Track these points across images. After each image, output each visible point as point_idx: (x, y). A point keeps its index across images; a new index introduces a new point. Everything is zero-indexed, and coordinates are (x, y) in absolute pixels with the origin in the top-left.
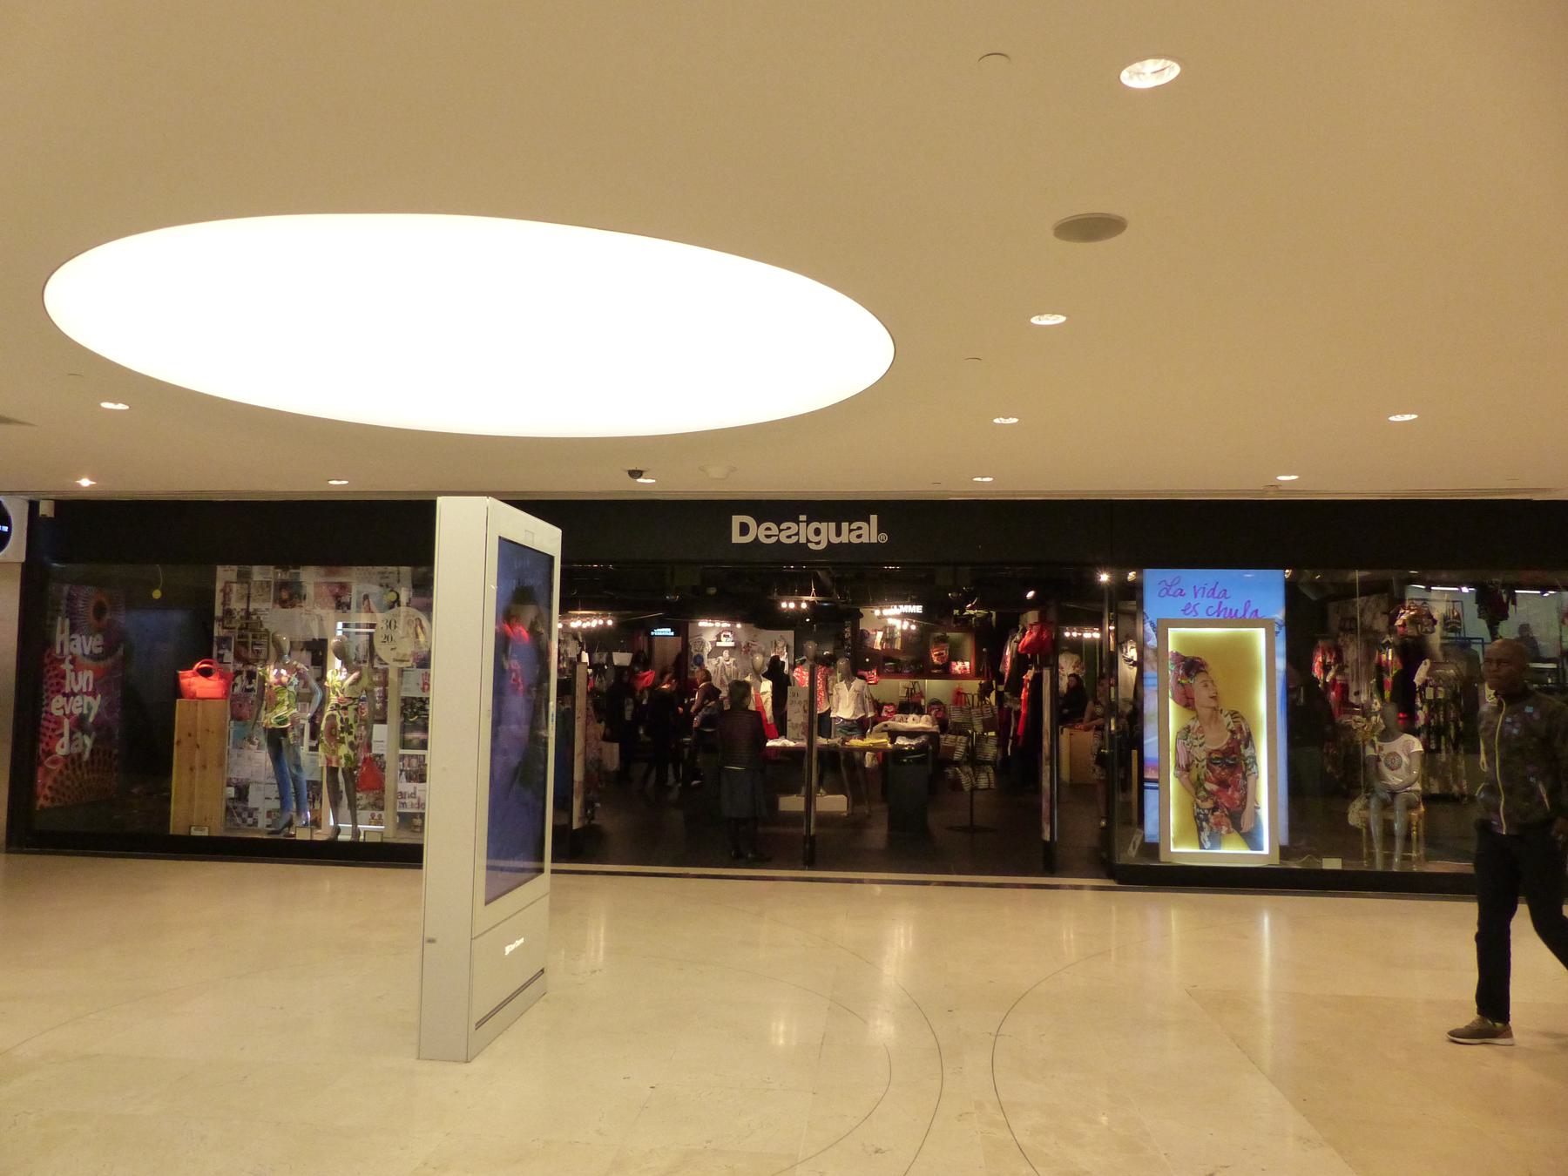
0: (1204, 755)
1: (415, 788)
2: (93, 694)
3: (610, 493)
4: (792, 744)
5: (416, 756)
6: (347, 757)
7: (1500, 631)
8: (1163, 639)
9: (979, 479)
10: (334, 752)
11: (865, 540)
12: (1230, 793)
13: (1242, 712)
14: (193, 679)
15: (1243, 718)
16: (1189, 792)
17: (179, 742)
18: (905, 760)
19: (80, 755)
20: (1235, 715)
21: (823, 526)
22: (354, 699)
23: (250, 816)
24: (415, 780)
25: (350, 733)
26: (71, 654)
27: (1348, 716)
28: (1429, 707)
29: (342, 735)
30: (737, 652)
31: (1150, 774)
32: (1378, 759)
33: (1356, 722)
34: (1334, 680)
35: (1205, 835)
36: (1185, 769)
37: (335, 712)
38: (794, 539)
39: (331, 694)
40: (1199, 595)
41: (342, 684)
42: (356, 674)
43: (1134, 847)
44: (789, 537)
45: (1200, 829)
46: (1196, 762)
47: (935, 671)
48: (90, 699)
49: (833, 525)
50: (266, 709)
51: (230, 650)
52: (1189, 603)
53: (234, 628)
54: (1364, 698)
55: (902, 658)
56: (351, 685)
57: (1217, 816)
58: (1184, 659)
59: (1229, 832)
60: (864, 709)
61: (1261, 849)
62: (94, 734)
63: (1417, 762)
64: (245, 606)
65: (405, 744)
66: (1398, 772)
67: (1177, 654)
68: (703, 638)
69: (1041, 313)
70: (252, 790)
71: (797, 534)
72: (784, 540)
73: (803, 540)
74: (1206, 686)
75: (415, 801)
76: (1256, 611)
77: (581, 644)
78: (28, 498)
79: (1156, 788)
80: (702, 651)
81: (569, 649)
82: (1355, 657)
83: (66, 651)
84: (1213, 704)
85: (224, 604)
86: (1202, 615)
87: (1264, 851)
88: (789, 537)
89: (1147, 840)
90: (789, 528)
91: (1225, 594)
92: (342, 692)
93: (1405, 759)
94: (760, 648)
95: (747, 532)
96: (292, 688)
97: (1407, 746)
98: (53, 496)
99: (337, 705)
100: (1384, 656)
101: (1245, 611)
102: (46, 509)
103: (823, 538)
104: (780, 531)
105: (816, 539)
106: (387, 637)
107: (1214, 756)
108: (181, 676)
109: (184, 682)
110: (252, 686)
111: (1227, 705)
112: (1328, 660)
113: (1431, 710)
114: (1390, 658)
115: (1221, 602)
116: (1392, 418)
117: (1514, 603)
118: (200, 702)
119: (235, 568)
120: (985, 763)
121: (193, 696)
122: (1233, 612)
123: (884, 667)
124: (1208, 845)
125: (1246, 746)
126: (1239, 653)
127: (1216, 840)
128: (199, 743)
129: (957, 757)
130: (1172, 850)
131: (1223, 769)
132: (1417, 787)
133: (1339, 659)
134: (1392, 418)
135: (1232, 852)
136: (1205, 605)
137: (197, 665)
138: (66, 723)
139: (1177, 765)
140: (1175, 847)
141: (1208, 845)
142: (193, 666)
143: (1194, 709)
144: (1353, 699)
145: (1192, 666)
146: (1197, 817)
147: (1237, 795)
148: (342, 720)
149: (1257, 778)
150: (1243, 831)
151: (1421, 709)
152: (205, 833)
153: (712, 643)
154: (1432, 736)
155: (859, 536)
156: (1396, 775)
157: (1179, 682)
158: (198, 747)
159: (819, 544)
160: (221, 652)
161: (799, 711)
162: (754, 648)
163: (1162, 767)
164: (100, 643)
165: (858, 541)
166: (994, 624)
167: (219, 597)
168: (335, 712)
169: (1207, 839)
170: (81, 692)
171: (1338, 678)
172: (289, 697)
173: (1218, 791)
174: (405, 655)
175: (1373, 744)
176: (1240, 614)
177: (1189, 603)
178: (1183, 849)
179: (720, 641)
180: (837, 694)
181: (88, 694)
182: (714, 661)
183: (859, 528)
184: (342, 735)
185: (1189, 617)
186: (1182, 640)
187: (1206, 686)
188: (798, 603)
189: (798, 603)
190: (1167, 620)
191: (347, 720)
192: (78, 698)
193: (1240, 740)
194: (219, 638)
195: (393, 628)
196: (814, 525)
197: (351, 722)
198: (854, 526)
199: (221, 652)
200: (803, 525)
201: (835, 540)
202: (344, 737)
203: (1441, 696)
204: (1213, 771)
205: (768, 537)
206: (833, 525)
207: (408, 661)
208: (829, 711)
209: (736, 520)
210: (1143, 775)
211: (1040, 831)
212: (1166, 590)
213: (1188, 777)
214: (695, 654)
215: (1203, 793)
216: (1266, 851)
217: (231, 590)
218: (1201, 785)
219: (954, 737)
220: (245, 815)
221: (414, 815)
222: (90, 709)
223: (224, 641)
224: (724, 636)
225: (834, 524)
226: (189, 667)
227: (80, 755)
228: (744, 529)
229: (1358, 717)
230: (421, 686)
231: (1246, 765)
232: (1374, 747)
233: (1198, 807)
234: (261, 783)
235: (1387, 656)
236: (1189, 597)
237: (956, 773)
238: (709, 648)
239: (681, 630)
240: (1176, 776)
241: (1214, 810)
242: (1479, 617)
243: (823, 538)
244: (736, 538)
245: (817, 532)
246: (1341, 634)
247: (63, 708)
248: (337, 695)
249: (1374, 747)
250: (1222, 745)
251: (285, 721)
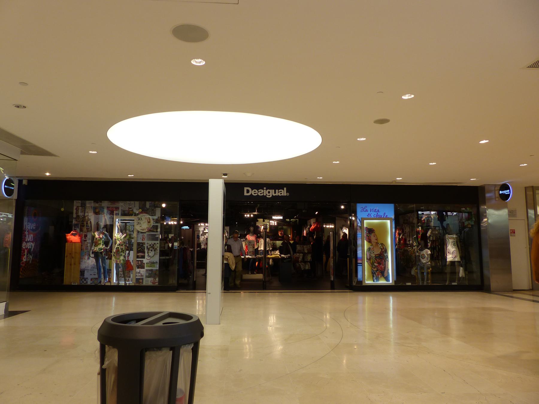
0: (374, 256)
1: (140, 270)
2: (32, 242)
3: (200, 180)
4: (251, 257)
5: (140, 261)
6: (123, 260)
8: (362, 223)
9: (318, 178)
10: (118, 259)
11: (283, 195)
12: (381, 266)
13: (384, 244)
14: (71, 237)
15: (384, 245)
16: (370, 266)
17: (67, 256)
19: (29, 261)
20: (382, 244)
21: (271, 191)
22: (125, 242)
23: (85, 280)
24: (140, 268)
25: (124, 253)
26: (28, 229)
27: (407, 247)
28: (431, 242)
29: (121, 253)
31: (359, 262)
32: (419, 256)
33: (409, 249)
34: (402, 237)
35: (375, 278)
36: (369, 259)
37: (119, 246)
38: (262, 194)
39: (117, 241)
40: (372, 211)
41: (121, 237)
42: (125, 235)
43: (355, 282)
44: (261, 194)
45: (373, 276)
46: (372, 258)
47: (280, 238)
48: (31, 243)
49: (273, 190)
50: (94, 246)
51: (78, 228)
52: (369, 214)
53: (80, 221)
54: (411, 242)
55: (269, 234)
56: (124, 238)
57: (378, 273)
58: (368, 229)
59: (381, 277)
61: (390, 281)
62: (33, 255)
63: (429, 256)
64: (83, 214)
65: (138, 257)
66: (425, 259)
67: (367, 227)
68: (199, 229)
69: (526, 165)
70: (86, 272)
71: (263, 193)
72: (259, 195)
73: (265, 195)
74: (374, 236)
75: (140, 274)
76: (387, 216)
78: (18, 178)
79: (361, 265)
80: (199, 234)
82: (409, 230)
83: (26, 228)
84: (376, 241)
85: (76, 213)
86: (372, 217)
87: (391, 281)
88: (261, 194)
89: (358, 280)
90: (261, 191)
91: (378, 211)
92: (121, 240)
93: (426, 256)
95: (248, 192)
96: (103, 239)
97: (427, 252)
98: (27, 179)
99: (119, 244)
100: (418, 229)
101: (384, 216)
102: (25, 182)
103: (271, 194)
104: (258, 192)
105: (269, 194)
107: (377, 256)
108: (66, 235)
109: (68, 237)
110: (86, 239)
111: (380, 242)
112: (400, 232)
113: (432, 243)
114: (420, 229)
115: (377, 213)
116: (430, 164)
117: (447, 216)
118: (73, 243)
119: (80, 201)
120: (308, 262)
121: (71, 242)
122: (381, 216)
124: (375, 280)
125: (385, 253)
126: (384, 226)
127: (378, 279)
128: (73, 256)
129: (300, 260)
130: (366, 282)
131: (379, 260)
132: (429, 263)
133: (403, 232)
134: (430, 164)
135: (382, 282)
136: (373, 214)
137: (72, 232)
138: (26, 250)
139: (367, 259)
140: (367, 281)
141: (375, 280)
142: (71, 232)
143: (371, 243)
144: (408, 243)
145: (370, 231)
146: (372, 273)
147: (383, 267)
148: (121, 248)
149: (388, 261)
150: (385, 277)
151: (429, 243)
152: (77, 284)
153: (202, 231)
154: (432, 250)
155: (281, 194)
156: (424, 260)
157: (367, 235)
158: (73, 258)
159: (269, 196)
160: (75, 229)
161: (251, 247)
163: (362, 259)
164: (35, 226)
165: (281, 195)
166: (298, 224)
167: (75, 211)
168: (119, 246)
169: (375, 279)
170: (30, 241)
171: (403, 237)
172: (103, 242)
173: (378, 265)
174: (144, 228)
175: (418, 252)
176: (382, 217)
177: (369, 214)
178: (369, 282)
179: (205, 230)
180: (261, 243)
181: (31, 242)
182: (203, 237)
183: (281, 191)
184: (121, 253)
185: (369, 217)
186: (368, 224)
187: (374, 236)
188: (250, 215)
189: (250, 215)
190: (364, 218)
191: (123, 248)
192: (29, 243)
193: (384, 251)
194: (75, 224)
195: (140, 220)
196: (268, 190)
197: (124, 249)
198: (280, 191)
199: (75, 229)
200: (265, 190)
201: (274, 195)
202: (122, 254)
203: (434, 239)
204: (376, 260)
205: (255, 194)
206: (273, 190)
207: (145, 230)
208: (258, 248)
209: (246, 189)
210: (357, 261)
211: (330, 278)
212: (363, 210)
213: (370, 262)
215: (374, 266)
216: (391, 282)
217: (79, 209)
218: (374, 264)
219: (299, 254)
220: (83, 280)
221: (140, 279)
222: (32, 247)
223: (76, 225)
224: (207, 229)
225: (274, 190)
226: (69, 233)
227: (29, 261)
228: (248, 191)
229: (409, 247)
230: (142, 239)
231: (385, 258)
232: (418, 253)
233: (373, 270)
234: (89, 270)
235: (419, 229)
236: (369, 212)
237: (300, 265)
238: (201, 233)
240: (367, 262)
241: (377, 271)
242: (438, 220)
243: (271, 194)
244: (246, 194)
245: (269, 192)
246: (404, 224)
247: (25, 246)
248: (119, 241)
249: (418, 253)
250: (379, 253)
251: (102, 249)
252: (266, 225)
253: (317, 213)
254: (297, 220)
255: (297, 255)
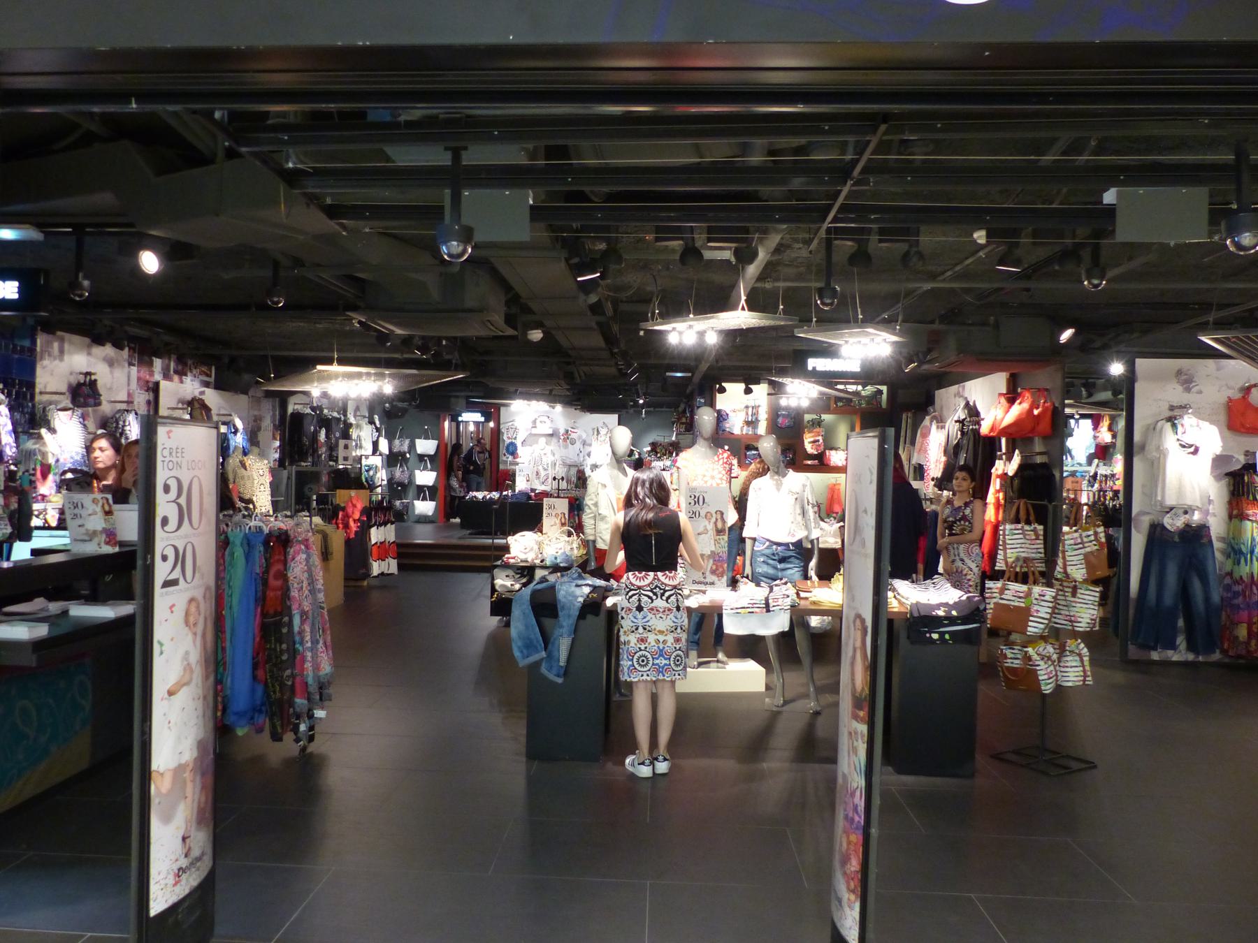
7: (840, 465)
18: (935, 636)
30: (554, 440)
60: (807, 527)
77: (378, 430)
81: (363, 434)
94: (580, 437)
106: (694, 513)
120: (1075, 635)
123: (746, 456)
129: (1034, 628)
162: (573, 436)
214: (508, 441)
219: (1024, 588)
237: (1028, 658)
239: (491, 413)
252: (755, 408)
253: (1070, 340)
254: (884, 388)
255: (1008, 595)
